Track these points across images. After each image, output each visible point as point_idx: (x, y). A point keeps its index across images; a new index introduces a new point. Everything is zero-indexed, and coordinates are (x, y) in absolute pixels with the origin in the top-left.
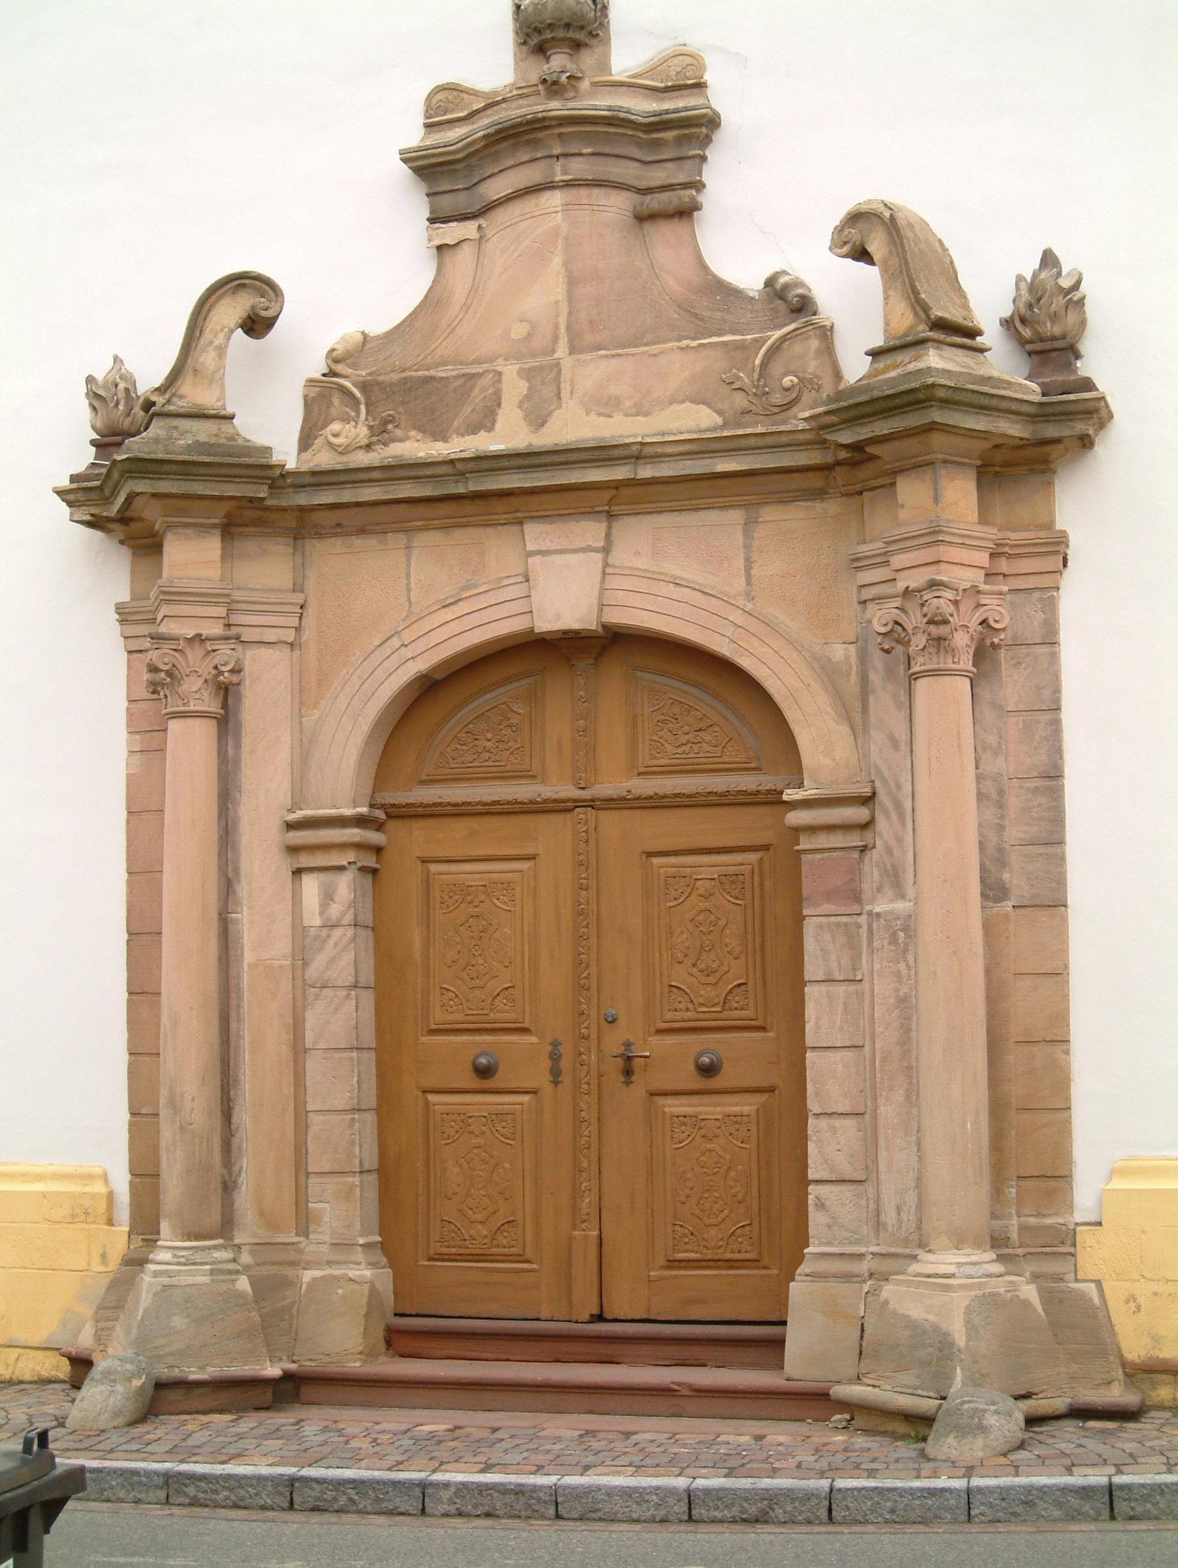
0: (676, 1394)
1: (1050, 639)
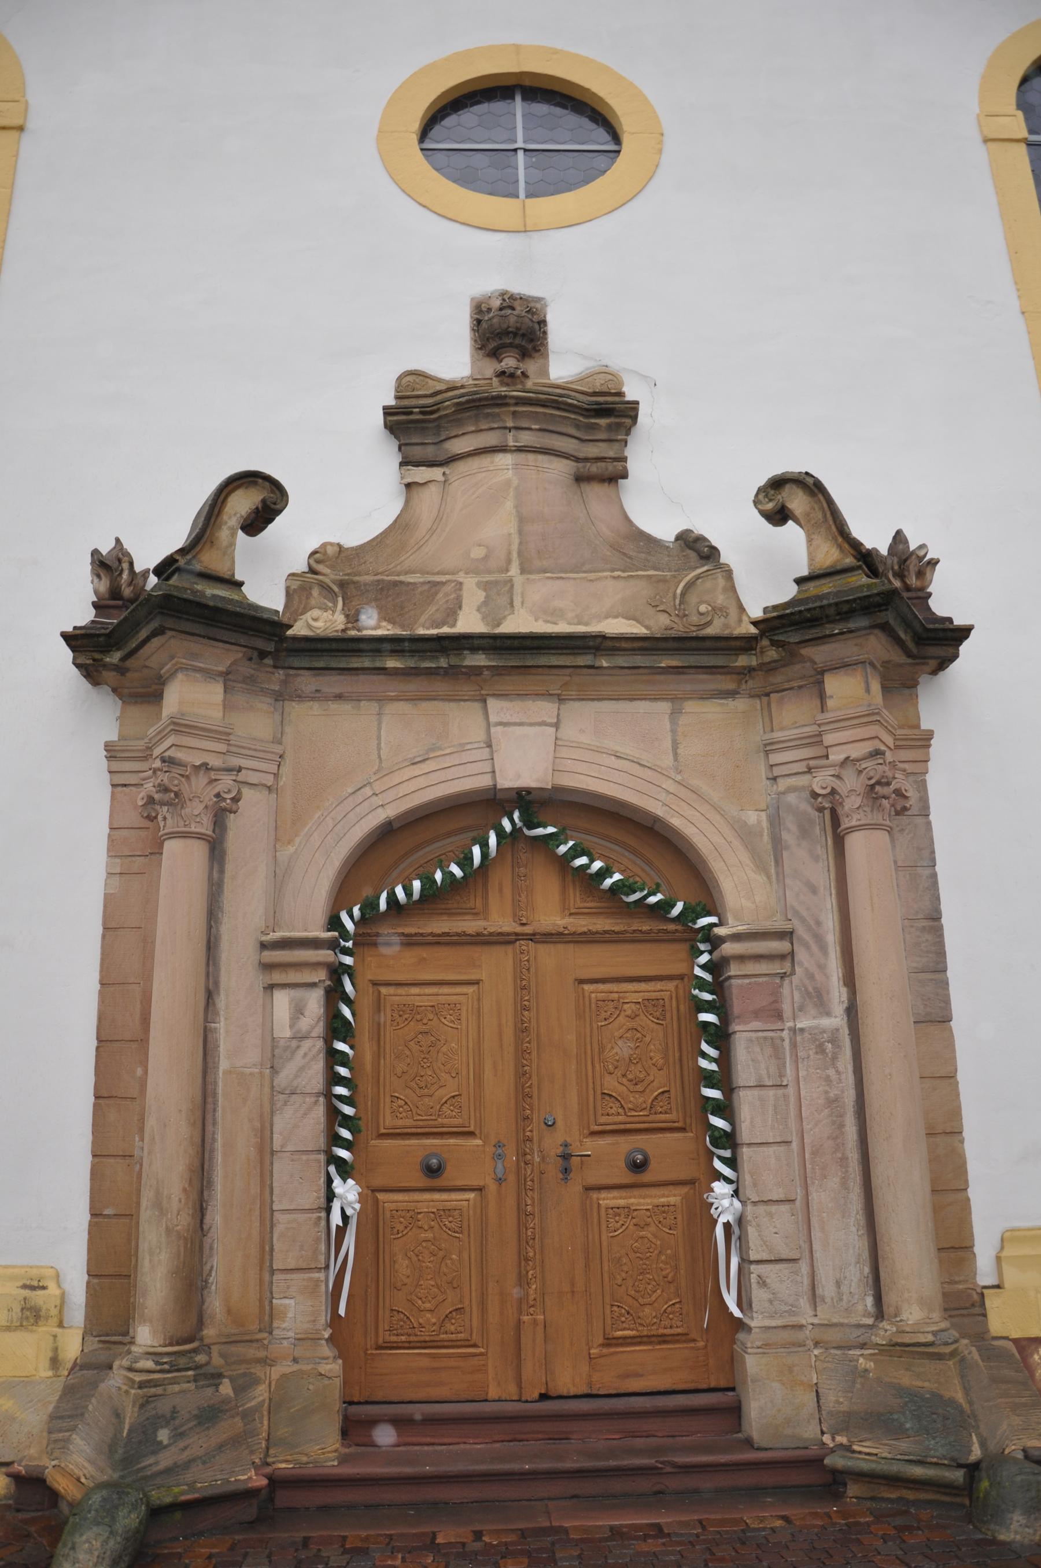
0: (660, 1471)
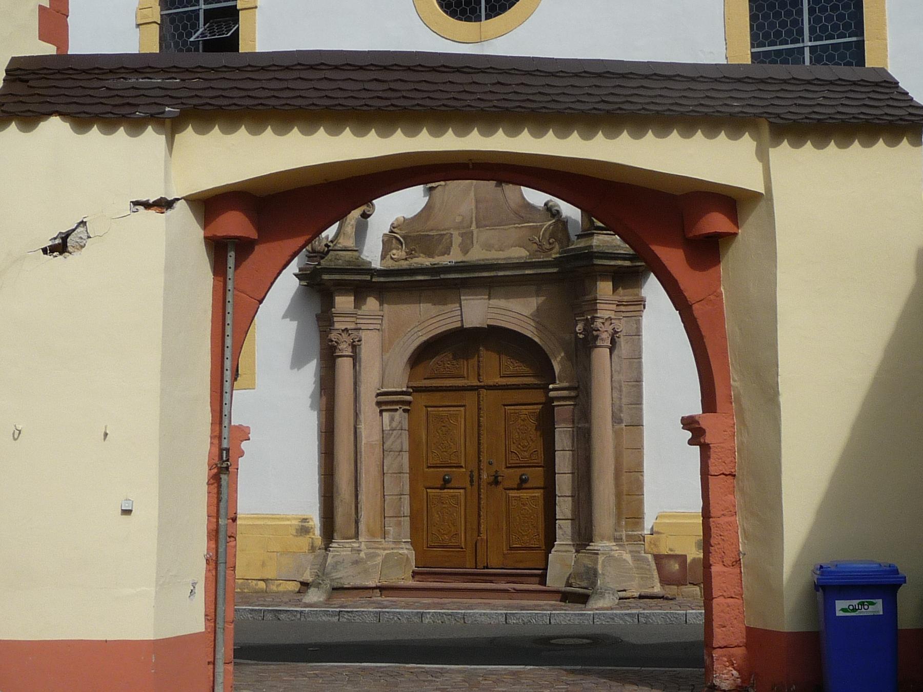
1: (638, 334)
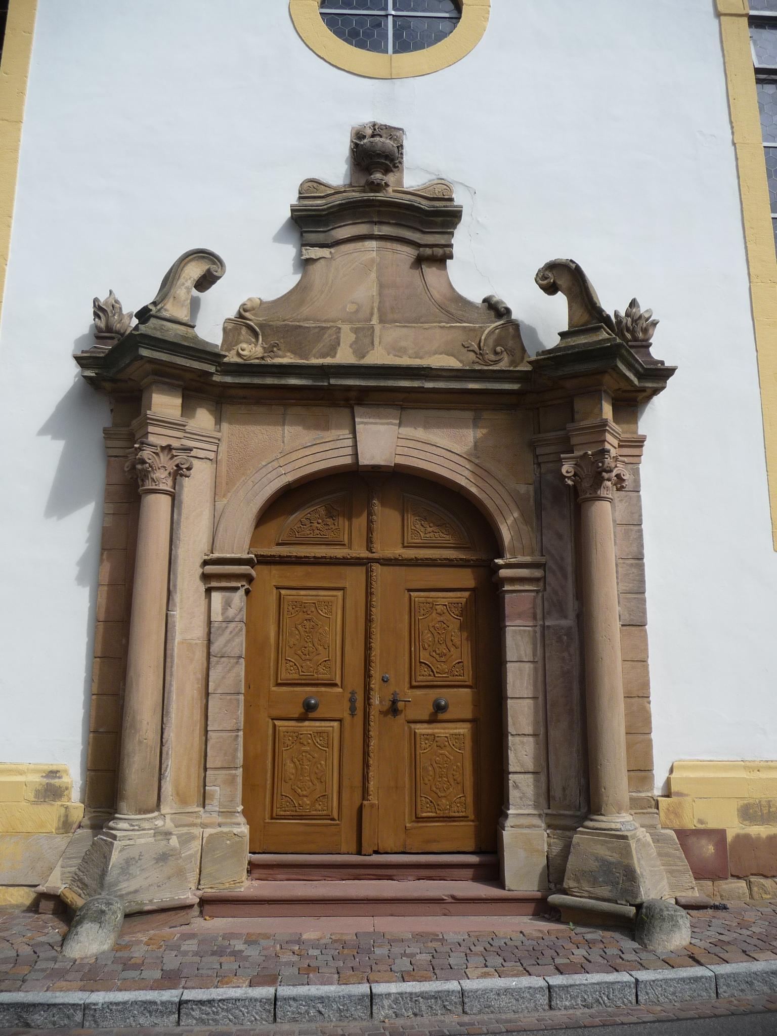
0: (445, 901)
